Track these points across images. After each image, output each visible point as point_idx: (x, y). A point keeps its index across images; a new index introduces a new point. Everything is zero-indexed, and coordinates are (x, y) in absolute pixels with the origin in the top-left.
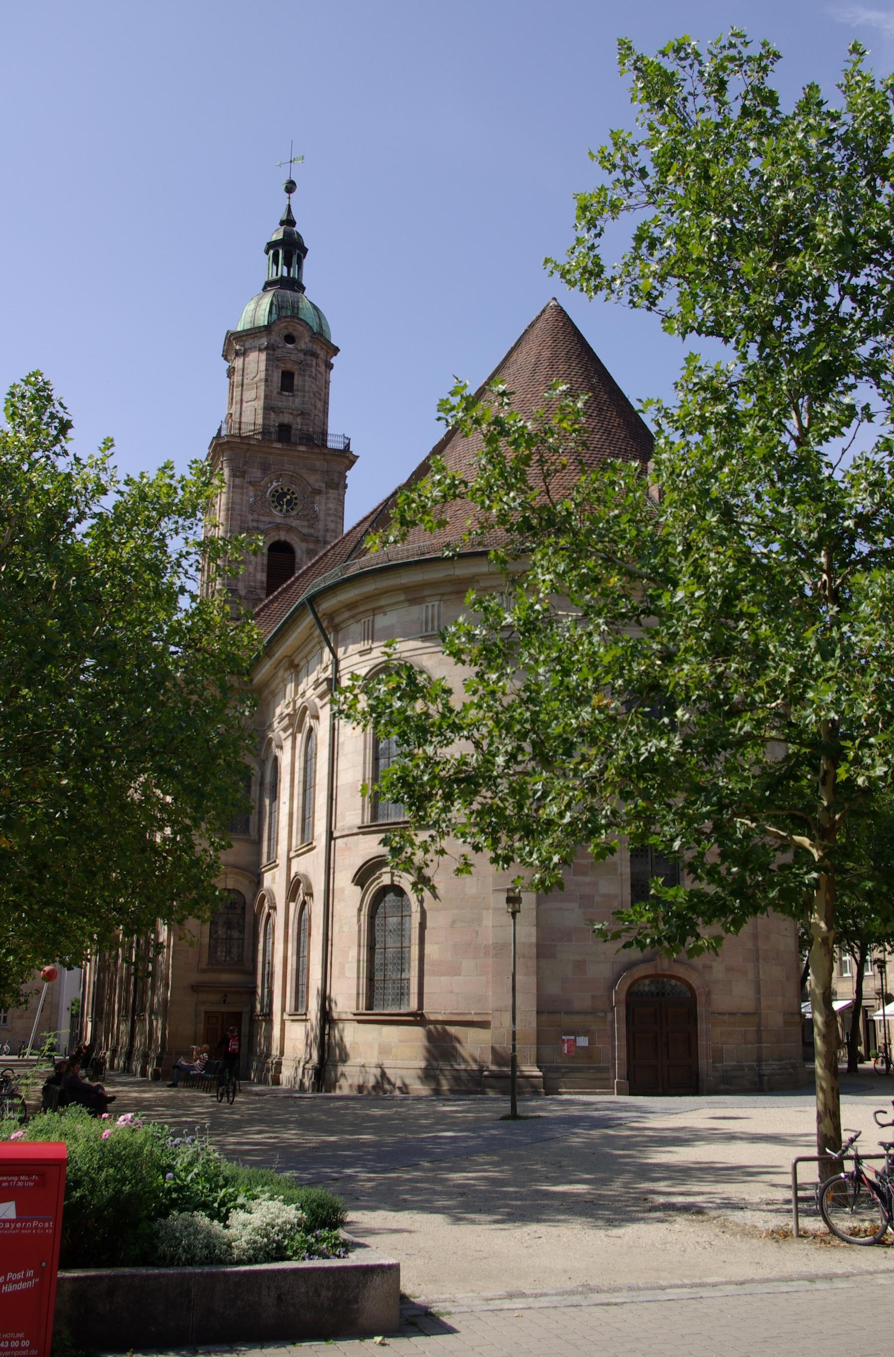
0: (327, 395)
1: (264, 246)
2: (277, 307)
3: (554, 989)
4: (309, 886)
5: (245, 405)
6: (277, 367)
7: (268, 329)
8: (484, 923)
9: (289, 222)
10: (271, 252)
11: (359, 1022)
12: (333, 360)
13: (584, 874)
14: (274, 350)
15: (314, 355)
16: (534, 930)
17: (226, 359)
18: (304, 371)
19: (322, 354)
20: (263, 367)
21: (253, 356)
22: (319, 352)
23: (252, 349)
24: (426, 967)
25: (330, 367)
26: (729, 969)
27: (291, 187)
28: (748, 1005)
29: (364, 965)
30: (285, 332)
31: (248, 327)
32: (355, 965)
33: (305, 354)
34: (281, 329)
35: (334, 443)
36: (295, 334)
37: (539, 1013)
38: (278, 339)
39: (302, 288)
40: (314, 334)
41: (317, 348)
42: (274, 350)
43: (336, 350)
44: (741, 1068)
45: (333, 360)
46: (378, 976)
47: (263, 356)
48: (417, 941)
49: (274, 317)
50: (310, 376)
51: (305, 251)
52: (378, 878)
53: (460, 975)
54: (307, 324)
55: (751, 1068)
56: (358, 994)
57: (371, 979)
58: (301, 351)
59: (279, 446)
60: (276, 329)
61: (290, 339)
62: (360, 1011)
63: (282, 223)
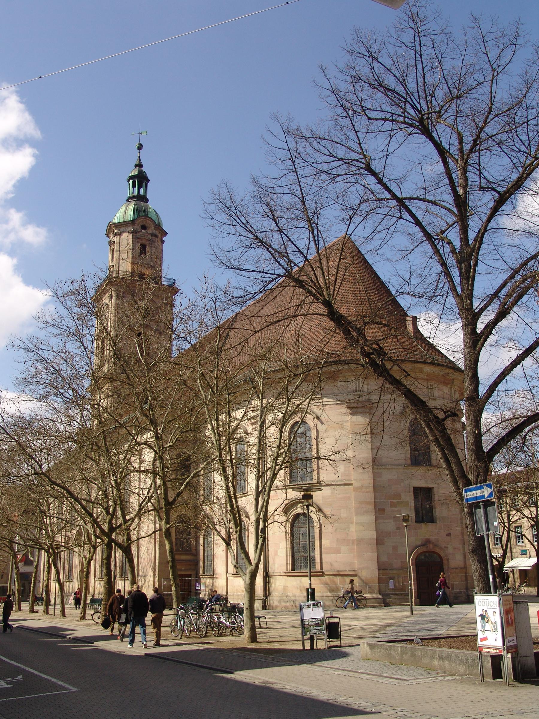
0: (162, 257)
1: (127, 177)
2: (138, 211)
3: (384, 559)
4: (246, 513)
5: (121, 262)
6: (138, 242)
7: (133, 222)
8: (351, 529)
9: (139, 165)
10: (131, 181)
11: (287, 576)
12: (164, 239)
13: (395, 506)
14: (136, 233)
15: (156, 236)
16: (375, 532)
17: (108, 236)
18: (151, 244)
19: (159, 235)
20: (131, 241)
21: (125, 235)
22: (158, 234)
23: (124, 232)
24: (323, 550)
25: (163, 242)
26: (454, 548)
27: (140, 147)
28: (461, 564)
29: (289, 550)
30: (142, 224)
31: (122, 220)
32: (285, 550)
33: (152, 236)
34: (139, 222)
35: (166, 282)
36: (146, 225)
37: (379, 569)
38: (138, 227)
39: (147, 201)
40: (157, 225)
41: (157, 233)
42: (136, 233)
43: (166, 234)
44: (461, 592)
45: (164, 239)
46: (297, 555)
47: (131, 236)
48: (318, 538)
49: (136, 216)
50: (154, 247)
51: (148, 181)
52: (296, 509)
53: (340, 553)
54: (153, 220)
55: (464, 593)
56: (287, 563)
57: (293, 556)
58: (150, 234)
59: (129, 646)
60: (137, 222)
61: (144, 227)
62: (289, 571)
63: (136, 166)
